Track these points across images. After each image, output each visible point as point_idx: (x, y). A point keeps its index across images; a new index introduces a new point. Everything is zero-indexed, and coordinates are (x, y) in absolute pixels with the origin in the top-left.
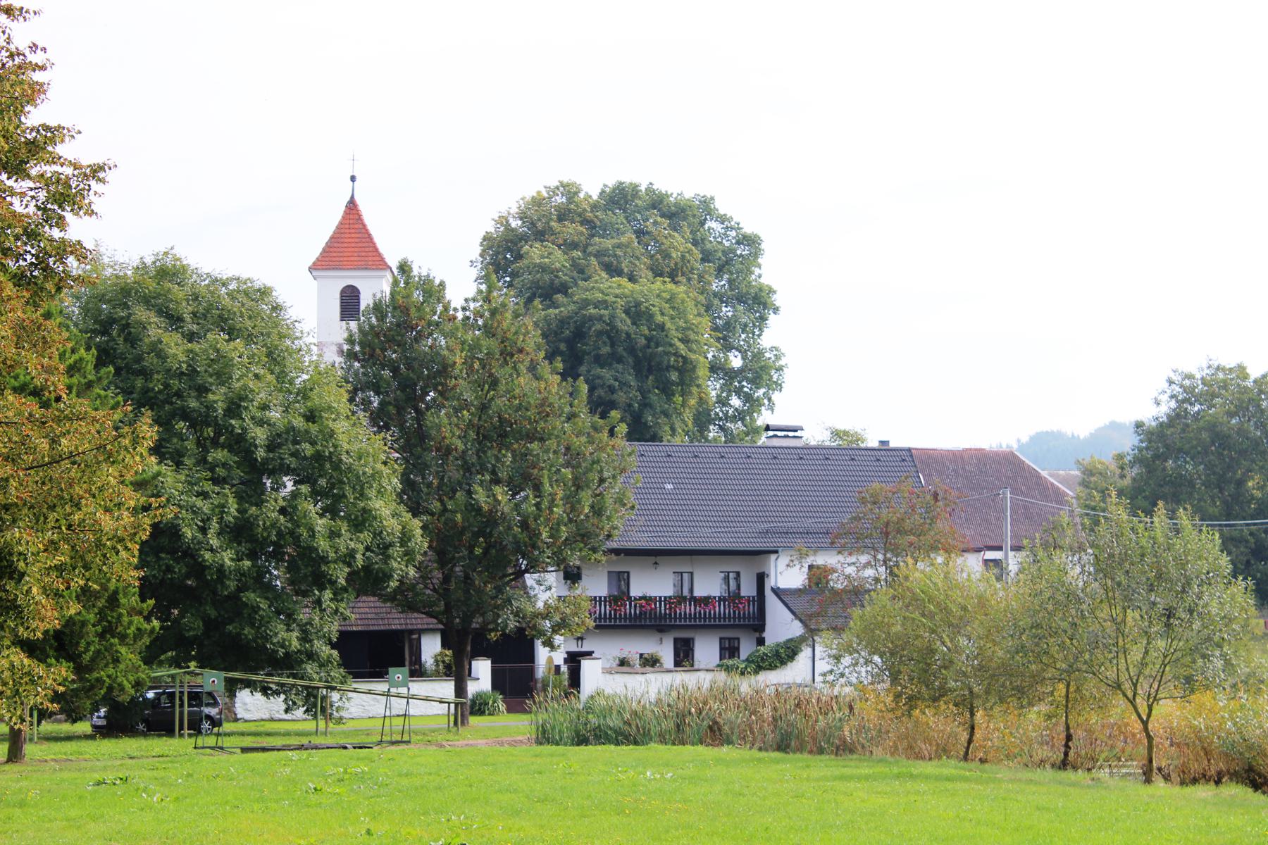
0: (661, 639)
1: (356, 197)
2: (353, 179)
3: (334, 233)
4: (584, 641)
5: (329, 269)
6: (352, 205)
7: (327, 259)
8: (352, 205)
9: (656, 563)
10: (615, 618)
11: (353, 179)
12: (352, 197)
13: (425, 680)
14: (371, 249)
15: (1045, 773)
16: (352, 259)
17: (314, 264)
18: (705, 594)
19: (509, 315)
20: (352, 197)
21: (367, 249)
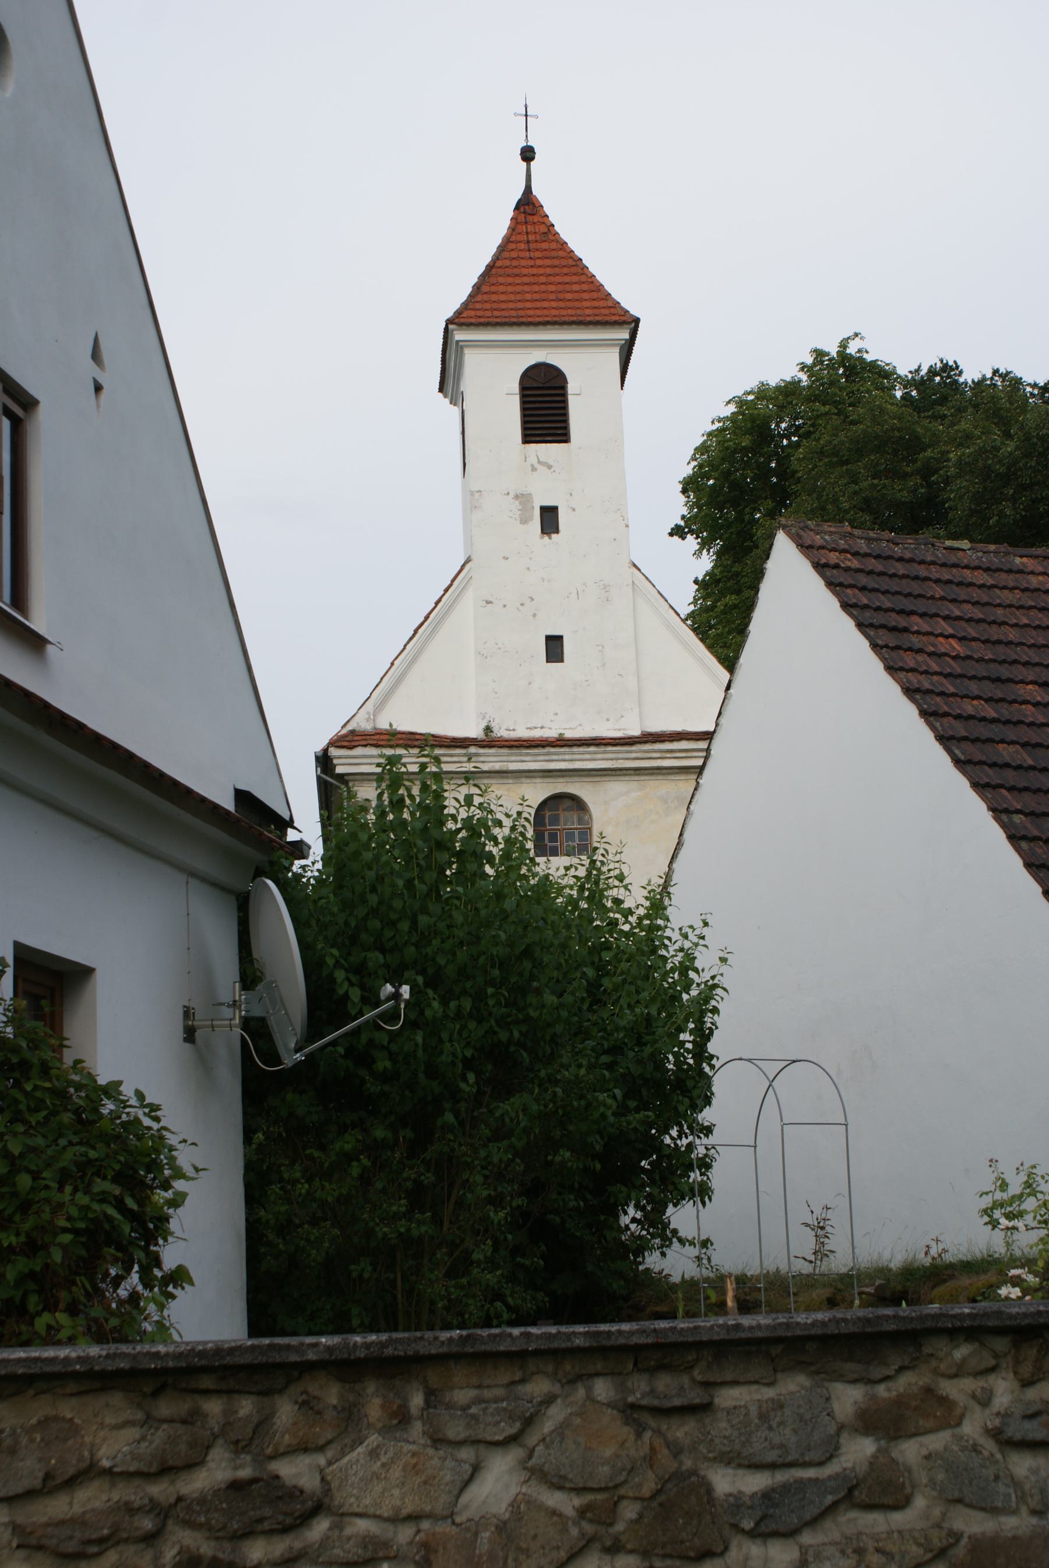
1: (535, 191)
2: (528, 154)
11: (528, 154)
12: (528, 189)
20: (528, 189)
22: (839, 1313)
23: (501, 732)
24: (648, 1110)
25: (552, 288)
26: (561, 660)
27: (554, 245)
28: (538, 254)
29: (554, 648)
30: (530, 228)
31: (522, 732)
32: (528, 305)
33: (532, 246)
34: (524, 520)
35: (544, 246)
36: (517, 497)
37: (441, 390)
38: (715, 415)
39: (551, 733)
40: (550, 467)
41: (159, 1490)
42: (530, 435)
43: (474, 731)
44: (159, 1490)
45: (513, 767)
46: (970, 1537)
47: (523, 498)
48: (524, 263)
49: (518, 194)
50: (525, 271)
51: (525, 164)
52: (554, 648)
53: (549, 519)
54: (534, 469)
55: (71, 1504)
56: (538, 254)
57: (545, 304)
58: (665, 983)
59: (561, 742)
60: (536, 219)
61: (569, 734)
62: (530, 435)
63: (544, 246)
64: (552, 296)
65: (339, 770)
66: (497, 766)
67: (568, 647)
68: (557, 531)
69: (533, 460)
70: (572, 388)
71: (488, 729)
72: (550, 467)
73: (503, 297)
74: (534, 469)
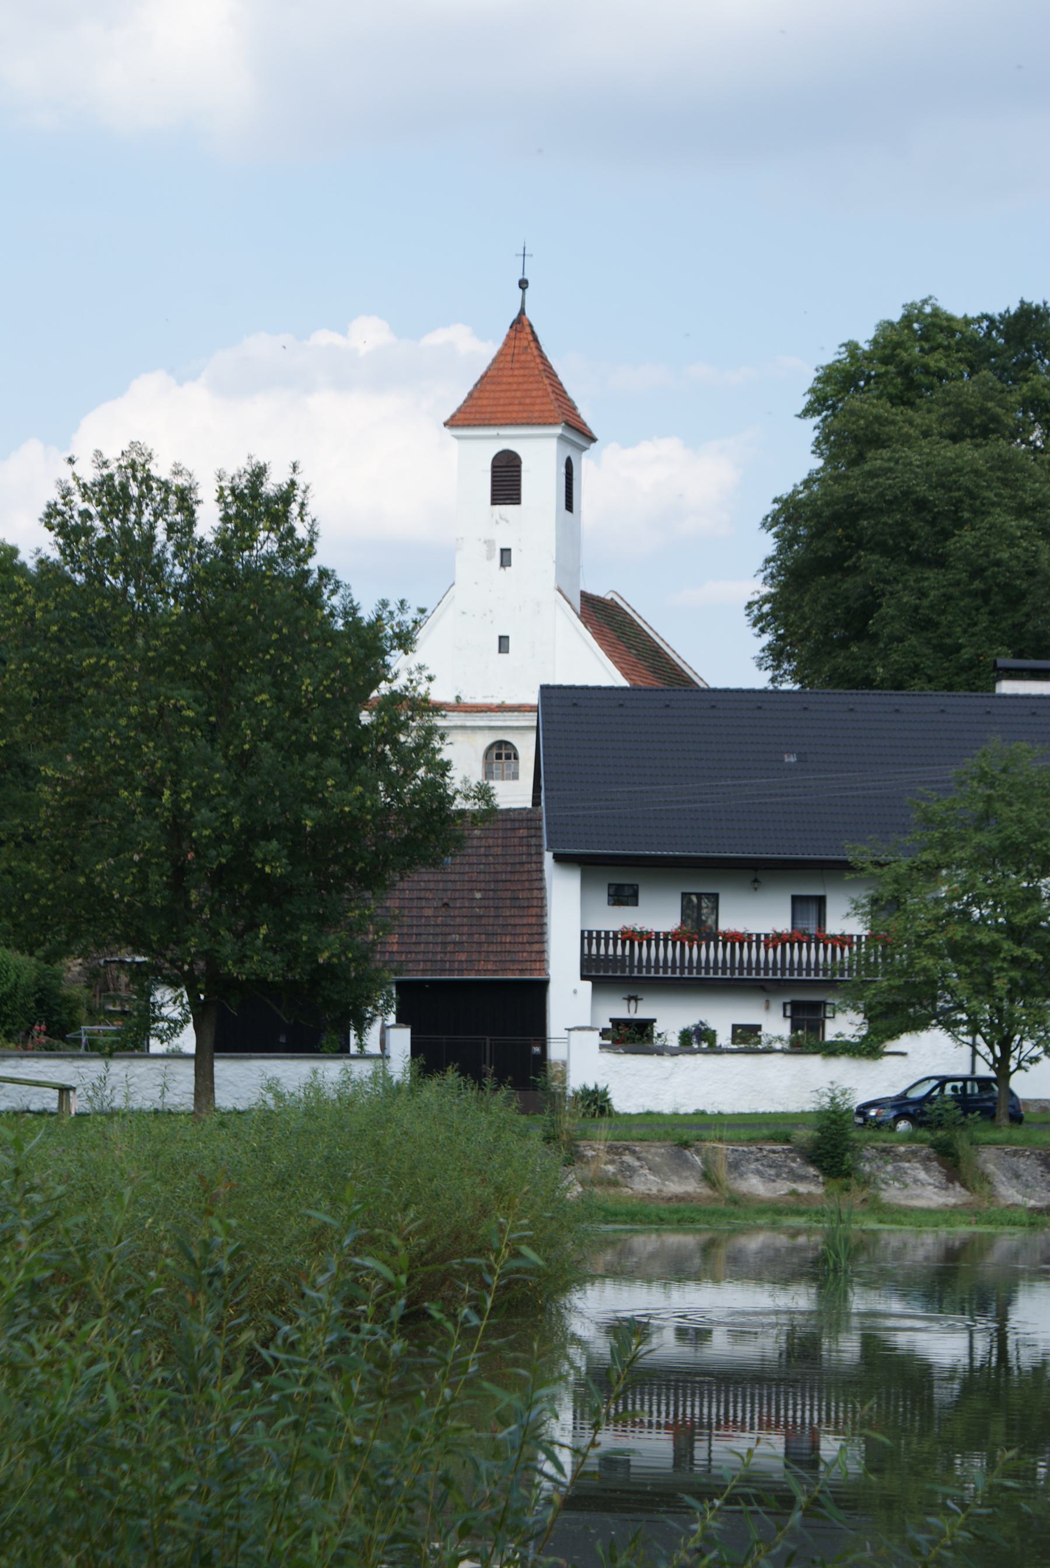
0: (767, 1002)
1: (529, 314)
2: (523, 284)
3: (489, 369)
4: (639, 1002)
5: (507, 424)
6: (520, 325)
7: (473, 410)
8: (520, 325)
9: (756, 881)
10: (682, 967)
11: (523, 284)
12: (522, 312)
13: (301, 1058)
14: (540, 393)
15: (95, 1075)
16: (510, 408)
17: (453, 417)
18: (838, 932)
19: (98, 523)
20: (522, 312)
21: (534, 394)
23: (466, 699)
24: (349, 967)
26: (507, 652)
29: (503, 644)
31: (479, 700)
34: (489, 558)
36: (485, 542)
38: (841, 343)
39: (496, 701)
40: (507, 521)
42: (496, 500)
43: (450, 699)
45: (468, 724)
47: (489, 543)
51: (521, 291)
52: (503, 644)
53: (506, 557)
54: (497, 523)
55: (562, 1445)
59: (502, 708)
61: (510, 701)
62: (496, 500)
66: (459, 723)
67: (512, 644)
68: (510, 565)
69: (497, 517)
70: (524, 467)
71: (458, 698)
72: (507, 521)
74: (497, 523)
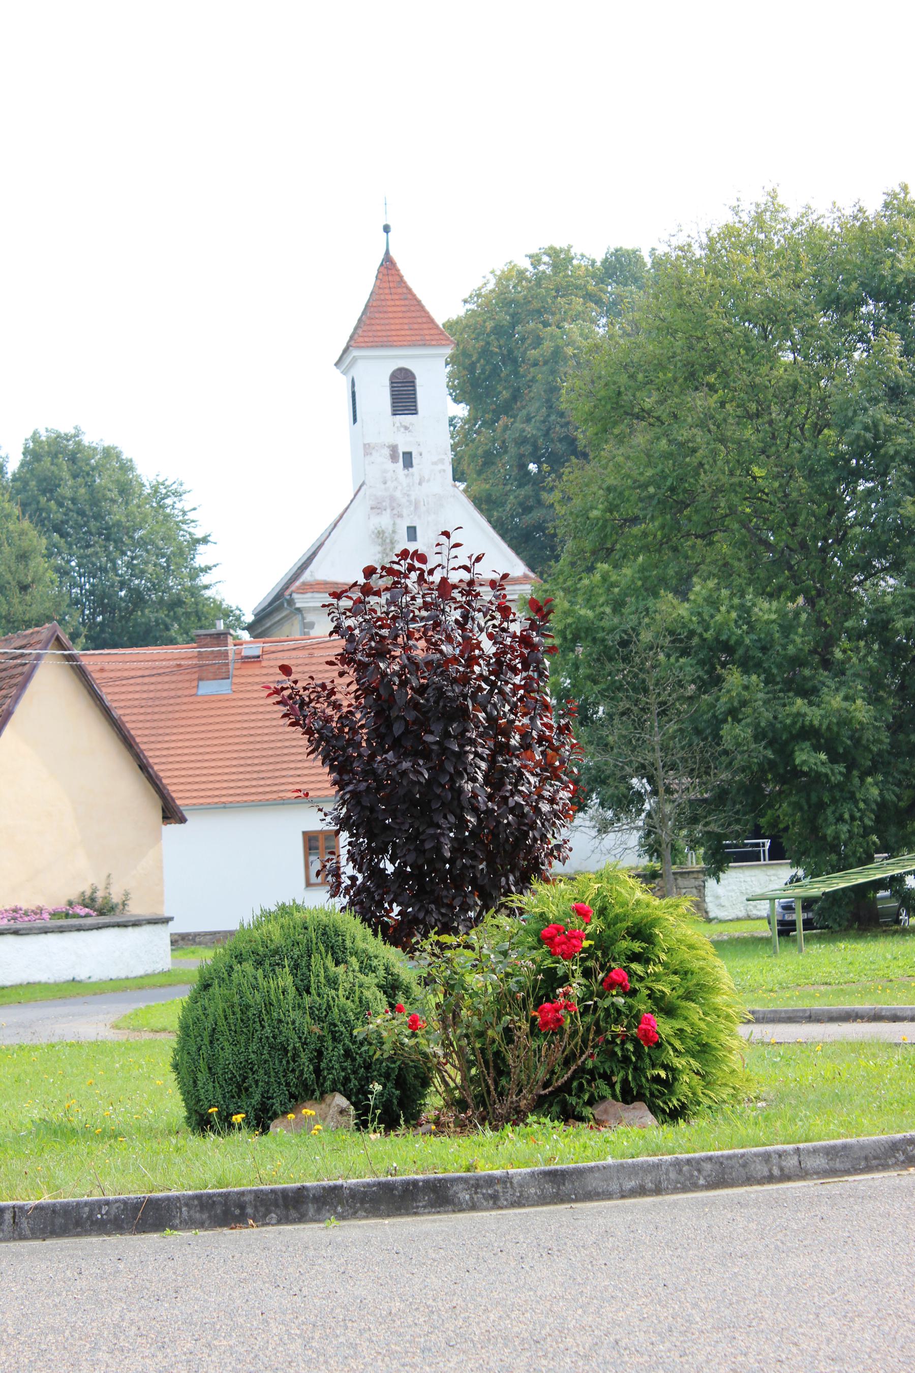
1: (392, 253)
2: (387, 229)
11: (387, 229)
22: (469, 1174)
25: (406, 321)
27: (405, 290)
28: (397, 297)
30: (391, 278)
32: (394, 333)
33: (393, 291)
35: (399, 291)
37: (336, 364)
41: (491, 1064)
44: (491, 1064)
46: (400, 1125)
48: (389, 303)
49: (381, 256)
50: (390, 309)
56: (397, 297)
57: (403, 333)
58: (503, 879)
60: (393, 272)
63: (399, 291)
64: (406, 327)
65: (298, 605)
69: (398, 424)
70: (418, 382)
73: (379, 328)
